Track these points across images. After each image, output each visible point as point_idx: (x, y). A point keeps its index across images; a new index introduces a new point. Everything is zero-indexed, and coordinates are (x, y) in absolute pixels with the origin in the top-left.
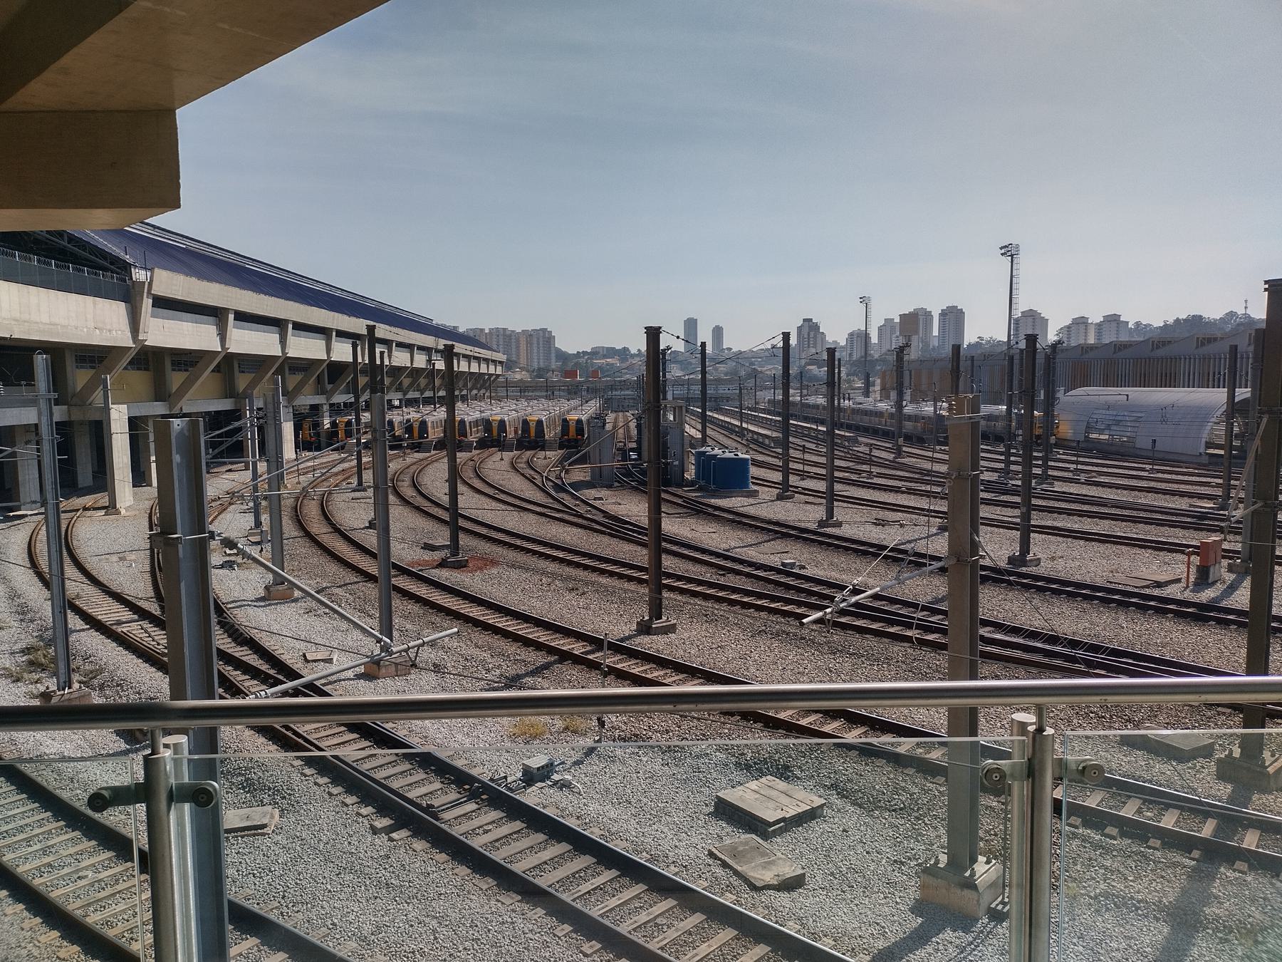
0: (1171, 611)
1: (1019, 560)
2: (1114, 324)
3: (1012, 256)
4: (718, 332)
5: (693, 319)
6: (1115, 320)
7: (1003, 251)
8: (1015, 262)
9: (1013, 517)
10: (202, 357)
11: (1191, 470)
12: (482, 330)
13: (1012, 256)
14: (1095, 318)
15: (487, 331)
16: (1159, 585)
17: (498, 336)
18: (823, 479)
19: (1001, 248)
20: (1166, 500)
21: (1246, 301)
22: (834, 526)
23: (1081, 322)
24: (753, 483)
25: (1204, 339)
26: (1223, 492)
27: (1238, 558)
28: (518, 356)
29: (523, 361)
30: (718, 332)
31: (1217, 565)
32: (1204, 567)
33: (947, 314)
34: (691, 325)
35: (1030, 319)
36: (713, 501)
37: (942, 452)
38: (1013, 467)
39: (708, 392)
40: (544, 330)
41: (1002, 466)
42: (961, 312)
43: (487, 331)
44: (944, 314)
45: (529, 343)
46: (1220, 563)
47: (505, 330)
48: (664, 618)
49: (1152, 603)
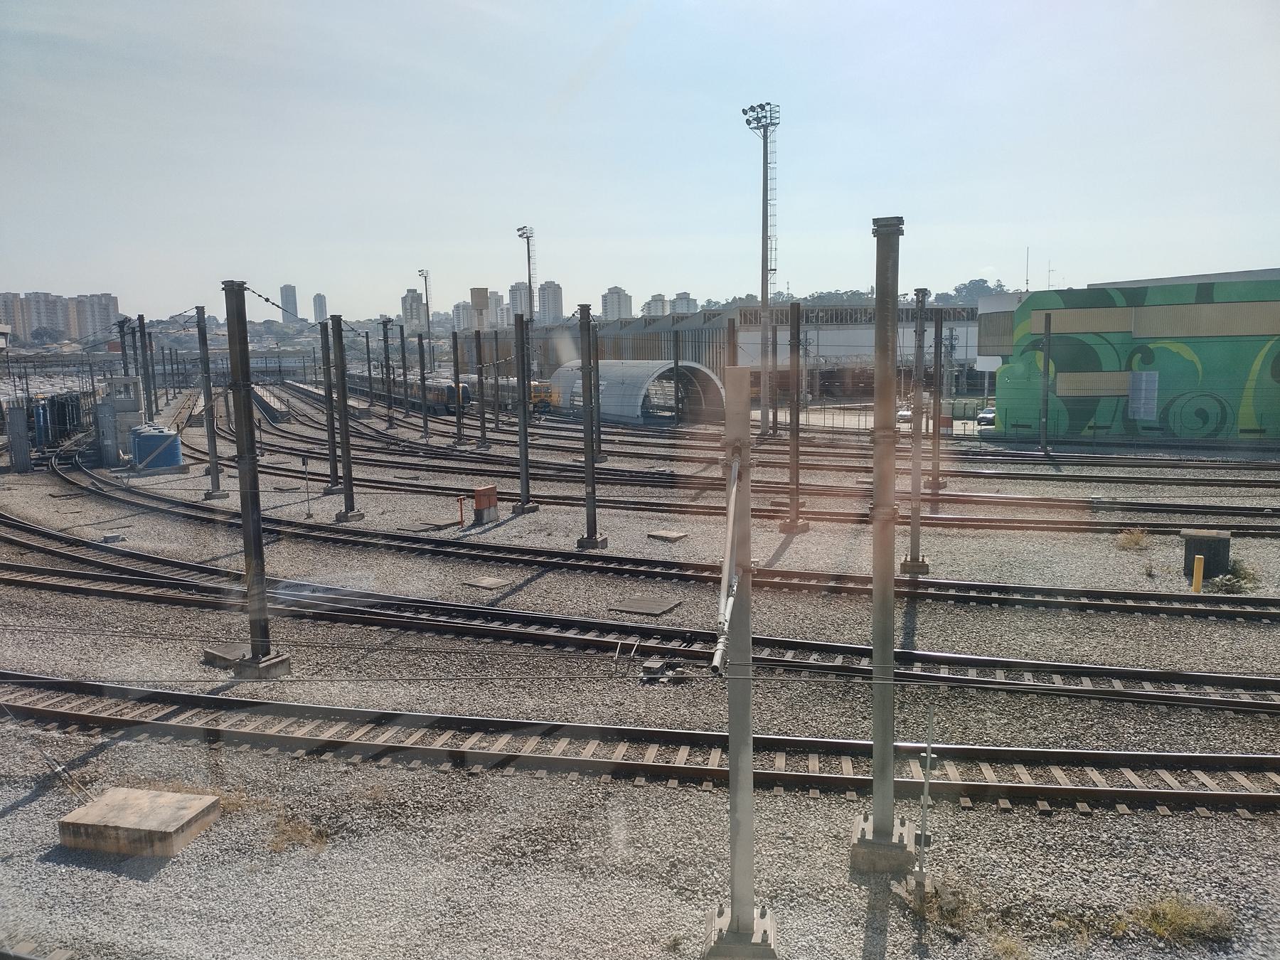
0: (973, 599)
1: (590, 540)
2: (685, 302)
3: (528, 238)
4: (320, 301)
5: (290, 286)
6: (686, 298)
7: (520, 233)
8: (531, 243)
9: (410, 478)
10: (699, 362)
11: (619, 430)
12: (16, 295)
13: (528, 238)
14: (670, 296)
15: (22, 296)
16: (439, 528)
17: (38, 302)
18: (325, 459)
19: (519, 230)
20: (618, 462)
21: (788, 282)
22: (219, 497)
23: (658, 299)
24: (752, 491)
25: (678, 317)
26: (585, 445)
27: (788, 518)
28: (67, 325)
29: (75, 333)
30: (320, 301)
31: (492, 508)
32: (478, 510)
33: (545, 289)
34: (289, 293)
35: (616, 296)
36: (135, 482)
37: (447, 423)
38: (467, 432)
39: (251, 365)
40: (107, 296)
41: (455, 430)
42: (558, 287)
43: (22, 296)
44: (543, 288)
45: (80, 313)
46: (496, 506)
47: (47, 295)
48: (273, 653)
49: (658, 570)
